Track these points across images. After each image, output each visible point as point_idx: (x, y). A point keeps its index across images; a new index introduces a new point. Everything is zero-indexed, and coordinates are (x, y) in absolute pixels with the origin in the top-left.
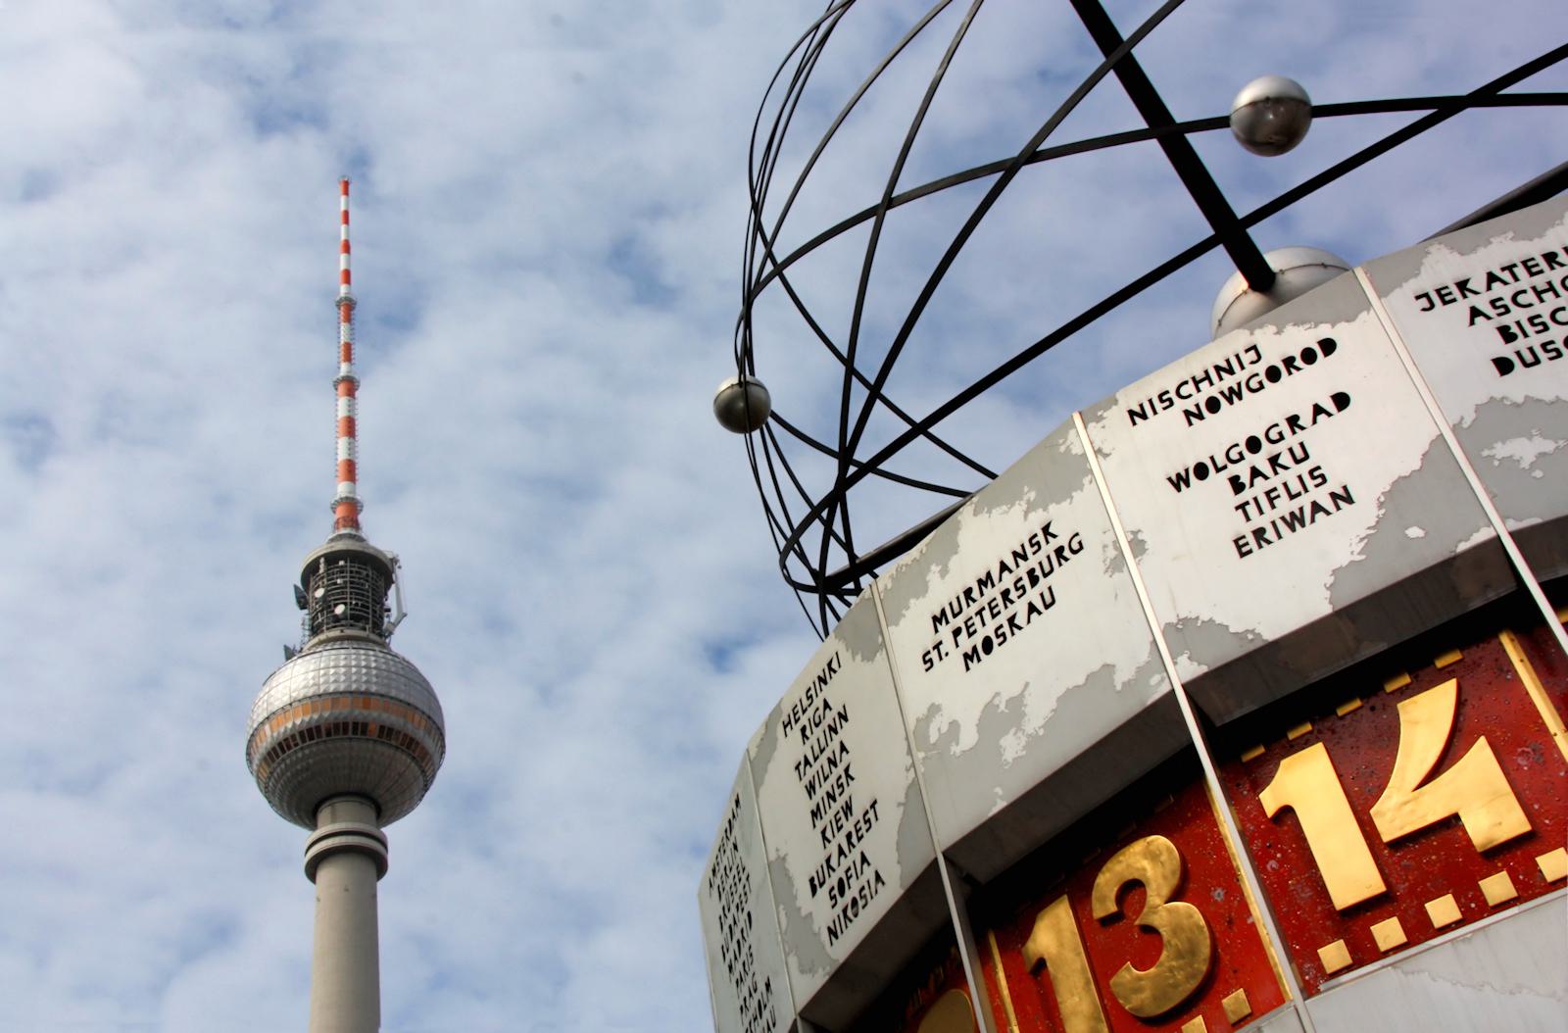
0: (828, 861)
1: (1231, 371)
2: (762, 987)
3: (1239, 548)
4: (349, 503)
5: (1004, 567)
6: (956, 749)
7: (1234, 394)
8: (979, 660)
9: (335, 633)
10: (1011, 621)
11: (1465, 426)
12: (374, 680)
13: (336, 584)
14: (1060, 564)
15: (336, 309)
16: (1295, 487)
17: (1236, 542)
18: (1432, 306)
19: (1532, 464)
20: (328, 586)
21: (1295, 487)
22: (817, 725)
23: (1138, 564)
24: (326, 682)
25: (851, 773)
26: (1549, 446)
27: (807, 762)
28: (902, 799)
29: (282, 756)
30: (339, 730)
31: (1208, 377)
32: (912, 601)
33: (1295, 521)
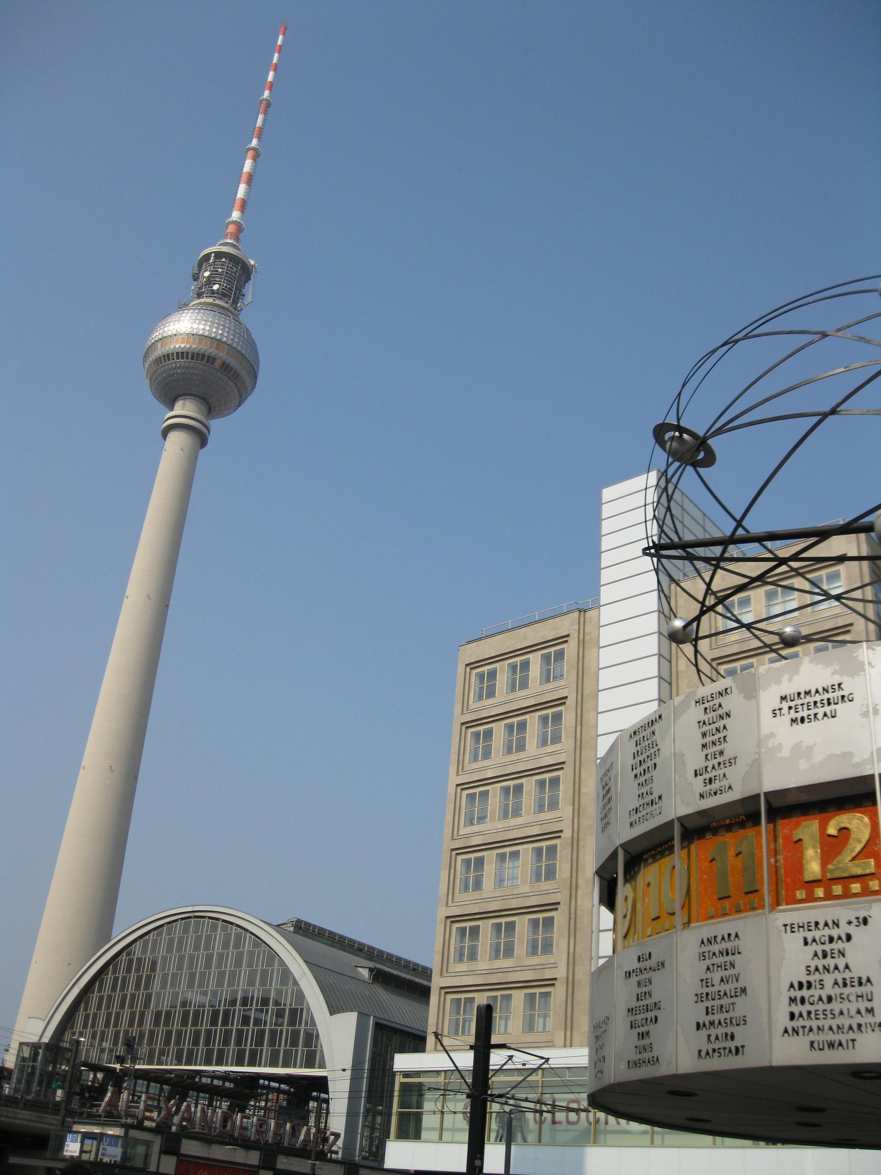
4: (237, 225)
5: (817, 692)
6: (778, 755)
8: (797, 724)
9: (210, 300)
10: (815, 715)
13: (217, 271)
20: (213, 271)
23: (874, 718)
25: (726, 739)
28: (750, 763)
29: (164, 363)
30: (204, 359)
32: (773, 686)
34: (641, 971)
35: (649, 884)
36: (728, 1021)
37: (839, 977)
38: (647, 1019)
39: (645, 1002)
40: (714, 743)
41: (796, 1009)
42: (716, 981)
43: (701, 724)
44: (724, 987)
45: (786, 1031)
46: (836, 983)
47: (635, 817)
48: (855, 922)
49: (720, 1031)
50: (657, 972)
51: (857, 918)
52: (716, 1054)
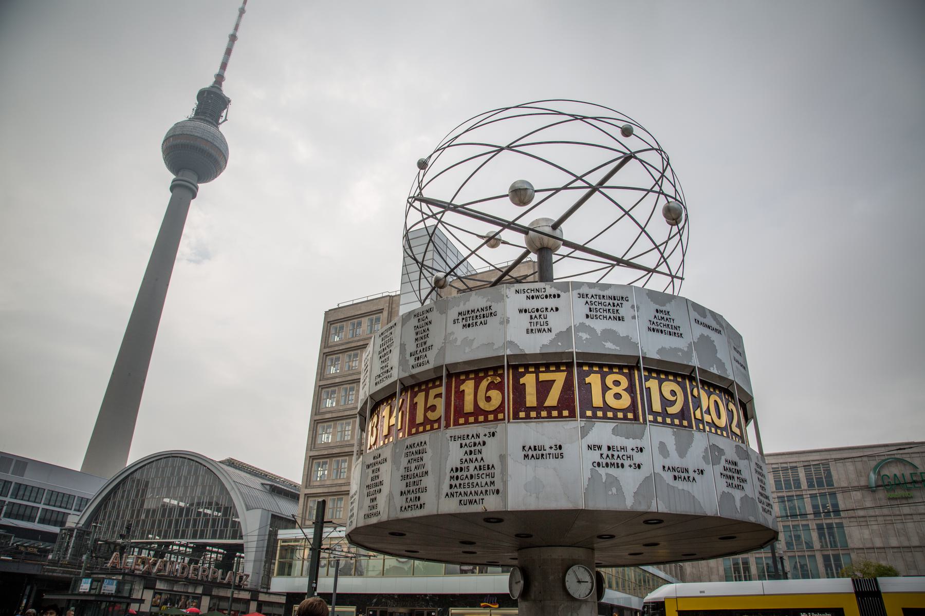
5: (478, 310)
7: (537, 297)
9: (203, 117)
10: (476, 323)
26: (588, 337)
31: (534, 290)
33: (539, 331)
34: (374, 464)
35: (384, 417)
36: (417, 490)
37: (477, 464)
38: (375, 491)
39: (375, 482)
40: (422, 338)
41: (454, 482)
42: (413, 468)
43: (652, 323)
44: (416, 472)
45: (447, 495)
46: (476, 468)
47: (378, 380)
48: (488, 435)
49: (413, 496)
50: (383, 464)
51: (490, 433)
52: (410, 509)
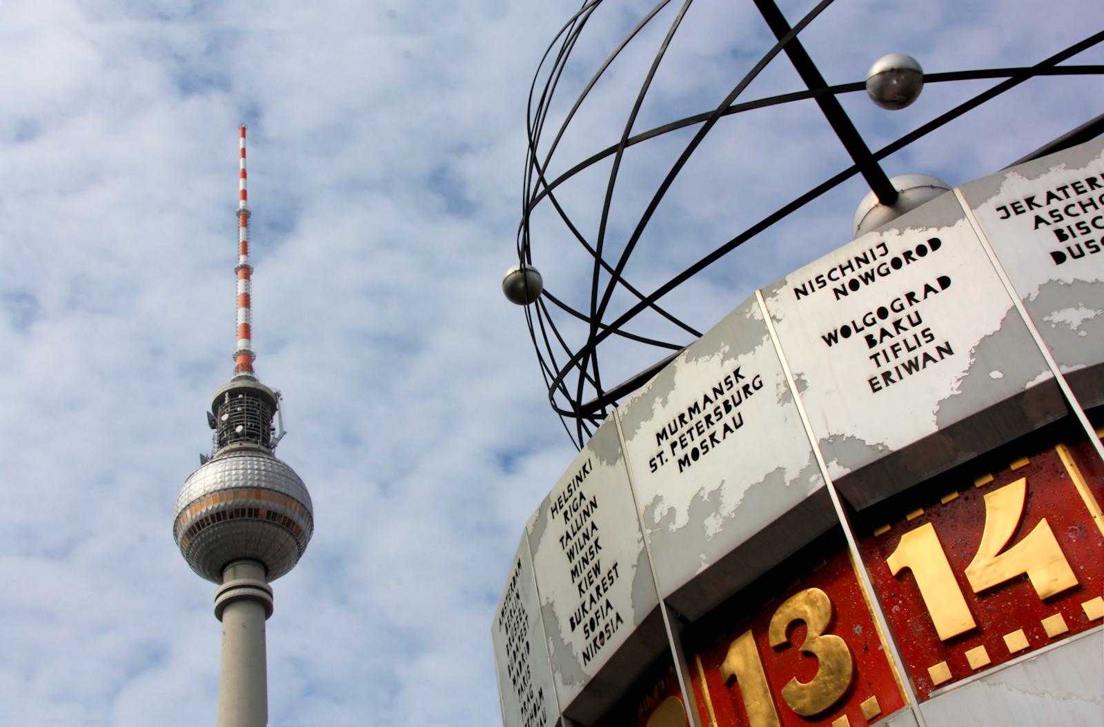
0: (583, 606)
1: (867, 261)
2: (536, 695)
3: (872, 385)
4: (246, 354)
5: (707, 399)
6: (673, 527)
7: (868, 278)
8: (689, 464)
9: (236, 445)
10: (712, 437)
11: (1032, 300)
12: (264, 478)
13: (236, 411)
14: (747, 397)
15: (237, 217)
16: (912, 343)
17: (870, 381)
18: (1008, 215)
19: (1079, 327)
20: (231, 412)
21: (912, 343)
22: (575, 510)
23: (801, 397)
24: (229, 480)
25: (599, 544)
26: (1090, 314)
27: (568, 536)
28: (635, 562)
29: (198, 532)
30: (239, 514)
31: (850, 266)
32: (642, 423)
33: (912, 366)
